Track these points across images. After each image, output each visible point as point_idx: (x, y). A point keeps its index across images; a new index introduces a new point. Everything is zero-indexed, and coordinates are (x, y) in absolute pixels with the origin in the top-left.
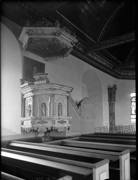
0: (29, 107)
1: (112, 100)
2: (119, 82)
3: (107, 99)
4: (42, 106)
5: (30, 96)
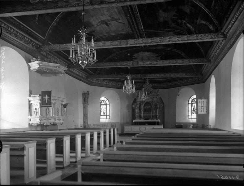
1: (86, 104)
2: (90, 88)
3: (82, 102)
4: (47, 110)
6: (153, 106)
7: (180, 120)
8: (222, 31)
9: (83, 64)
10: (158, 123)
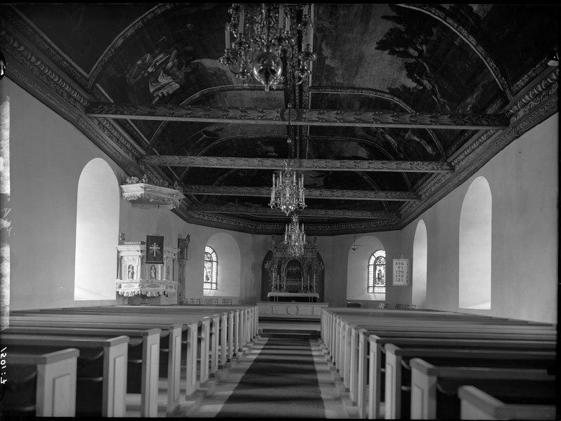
6: (305, 269)
7: (352, 296)
8: (449, 160)
9: (287, 211)
10: (314, 300)
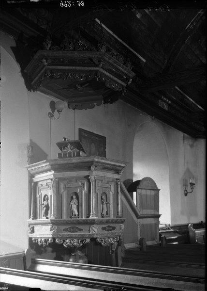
0: (44, 200)
5: (48, 179)
